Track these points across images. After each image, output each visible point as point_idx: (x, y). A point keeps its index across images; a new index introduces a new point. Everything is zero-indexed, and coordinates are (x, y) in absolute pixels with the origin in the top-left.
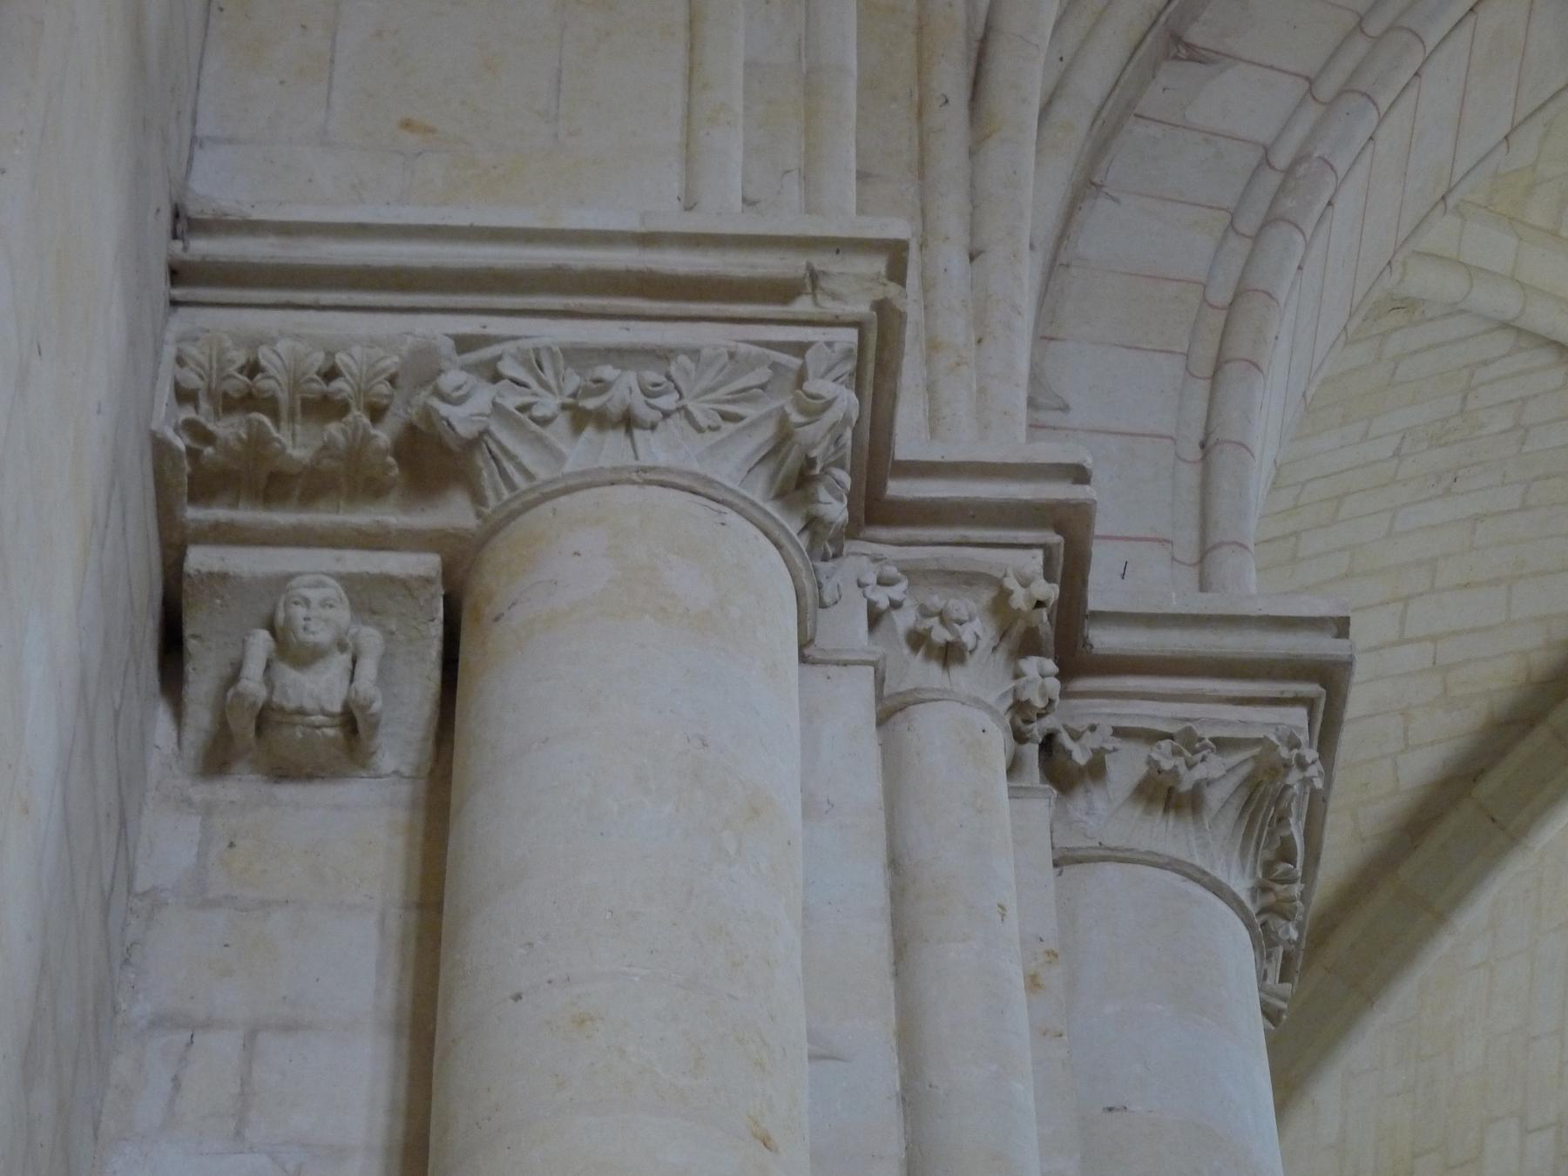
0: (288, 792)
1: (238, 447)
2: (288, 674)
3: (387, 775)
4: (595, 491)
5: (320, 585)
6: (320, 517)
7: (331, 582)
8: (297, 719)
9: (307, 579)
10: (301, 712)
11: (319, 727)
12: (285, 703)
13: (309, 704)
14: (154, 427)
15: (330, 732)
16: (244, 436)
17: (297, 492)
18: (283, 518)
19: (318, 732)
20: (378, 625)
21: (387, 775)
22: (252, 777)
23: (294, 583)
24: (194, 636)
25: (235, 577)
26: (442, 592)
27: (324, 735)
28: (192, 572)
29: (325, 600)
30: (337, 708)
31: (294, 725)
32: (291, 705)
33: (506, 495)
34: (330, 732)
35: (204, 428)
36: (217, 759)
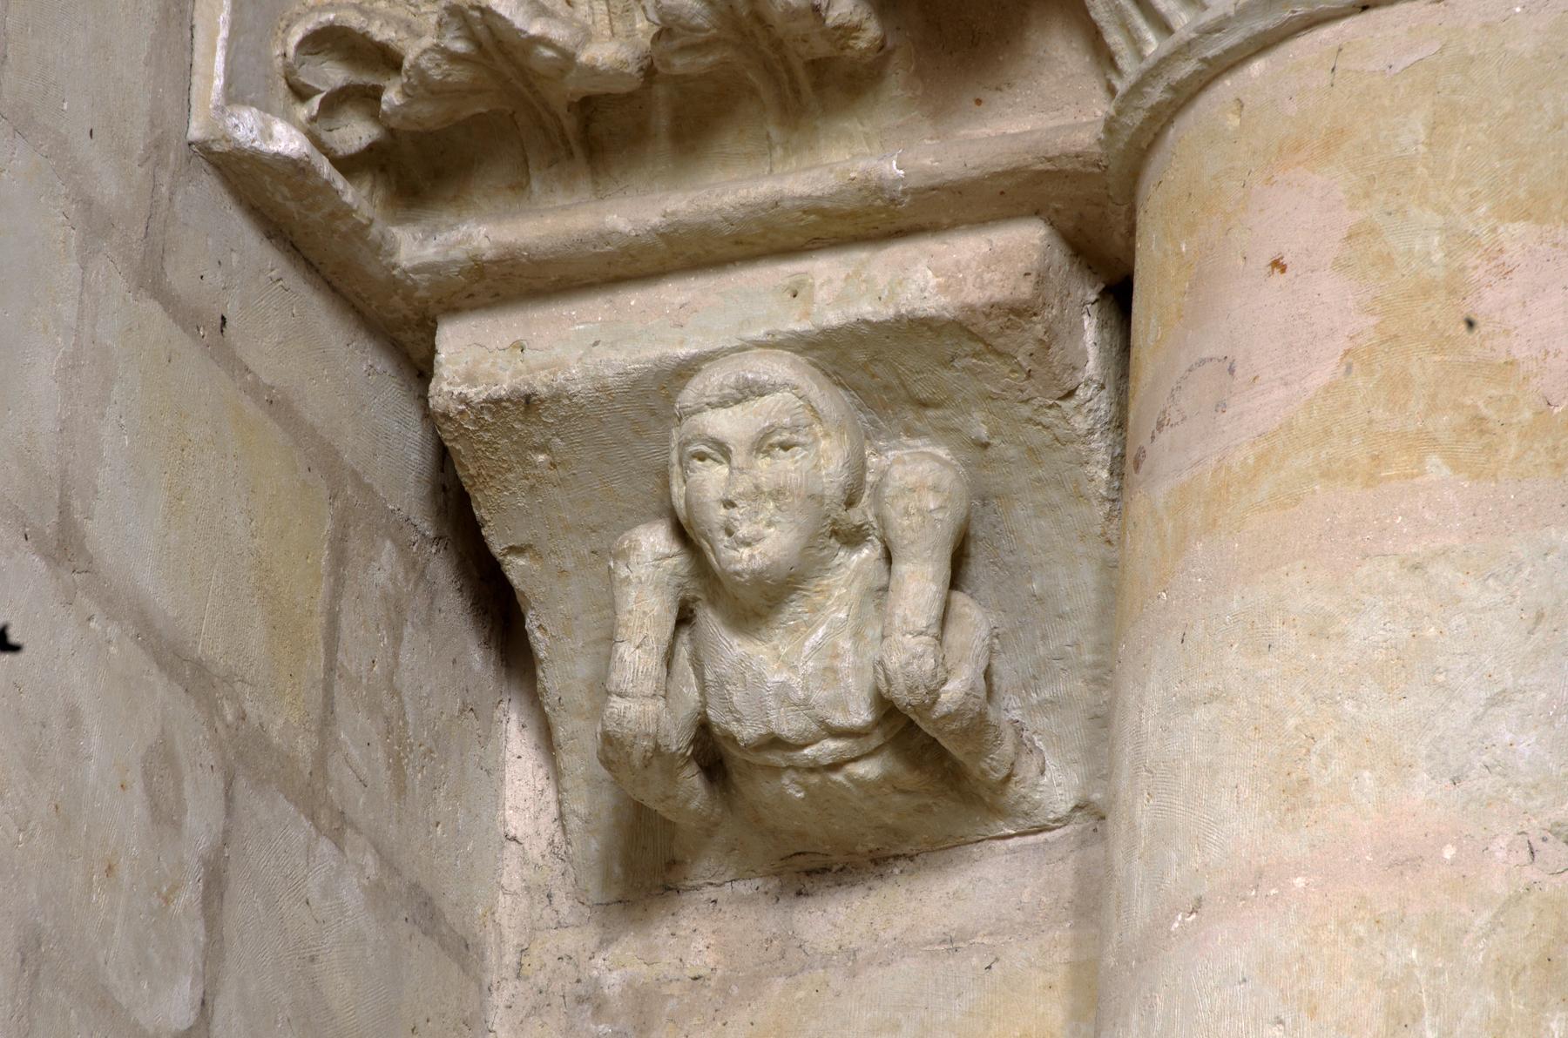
0: (836, 919)
1: (460, 75)
2: (734, 650)
3: (1062, 821)
4: (1325, 33)
5: (748, 391)
6: (729, 187)
7: (776, 367)
8: (776, 758)
9: (715, 379)
10: (775, 742)
11: (835, 766)
12: (734, 727)
13: (788, 725)
14: (196, 132)
15: (867, 770)
16: (460, 46)
17: (662, 121)
18: (631, 211)
19: (838, 777)
20: (945, 432)
21: (1062, 821)
22: (743, 888)
23: (689, 396)
24: (517, 550)
25: (556, 397)
26: (448, 917)
27: (860, 783)
28: (454, 408)
29: (767, 434)
30: (860, 714)
31: (777, 771)
32: (747, 731)
33: (1153, 44)
34: (867, 770)
35: (365, 36)
36: (644, 866)
